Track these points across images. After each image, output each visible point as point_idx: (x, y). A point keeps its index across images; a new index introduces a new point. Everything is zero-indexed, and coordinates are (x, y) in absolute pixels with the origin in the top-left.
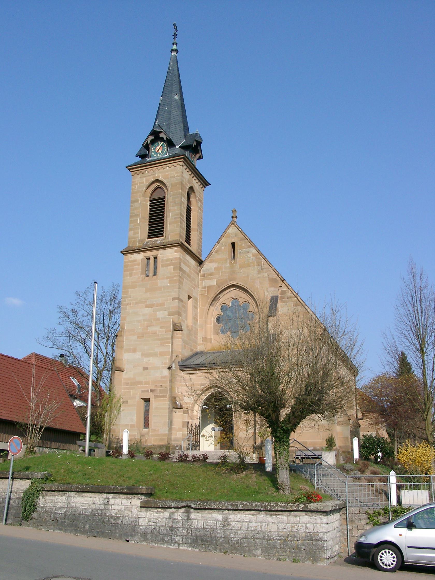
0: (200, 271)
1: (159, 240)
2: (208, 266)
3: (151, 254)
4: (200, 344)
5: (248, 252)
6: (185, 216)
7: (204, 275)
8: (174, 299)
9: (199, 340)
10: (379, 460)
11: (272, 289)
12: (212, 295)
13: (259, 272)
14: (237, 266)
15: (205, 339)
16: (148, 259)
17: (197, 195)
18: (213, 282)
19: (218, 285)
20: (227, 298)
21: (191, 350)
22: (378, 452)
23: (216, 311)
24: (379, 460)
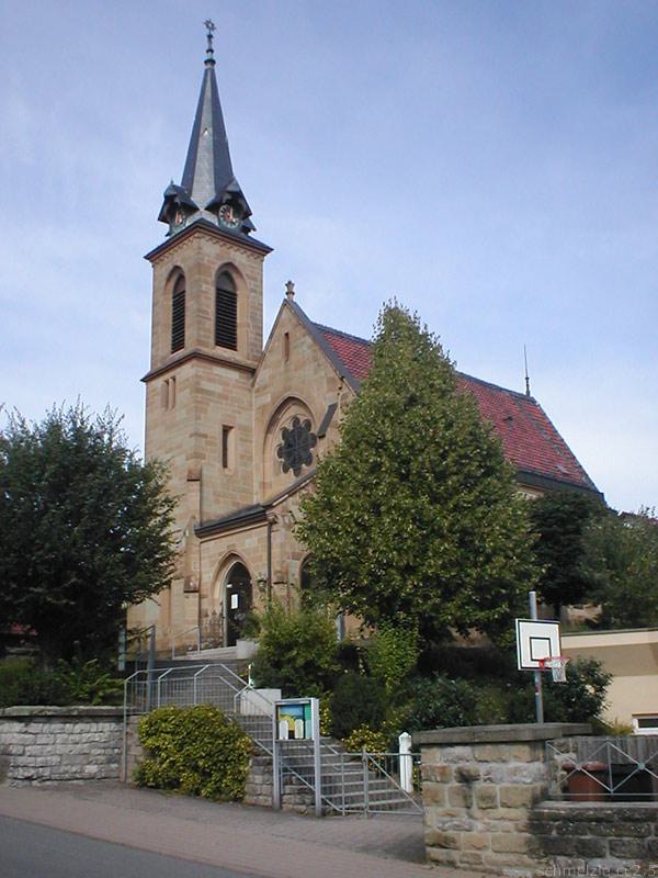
0: (253, 385)
1: (180, 353)
2: (263, 375)
3: (167, 376)
4: (257, 493)
5: (302, 343)
6: (188, 320)
7: (258, 391)
8: (191, 436)
9: (256, 487)
10: (122, 549)
11: (330, 394)
12: (267, 418)
13: (316, 372)
14: (292, 367)
15: (263, 485)
16: (167, 382)
17: (244, 272)
18: (268, 398)
19: (273, 400)
20: (285, 421)
21: (234, 504)
22: (433, 625)
23: (276, 439)
24: (122, 549)
